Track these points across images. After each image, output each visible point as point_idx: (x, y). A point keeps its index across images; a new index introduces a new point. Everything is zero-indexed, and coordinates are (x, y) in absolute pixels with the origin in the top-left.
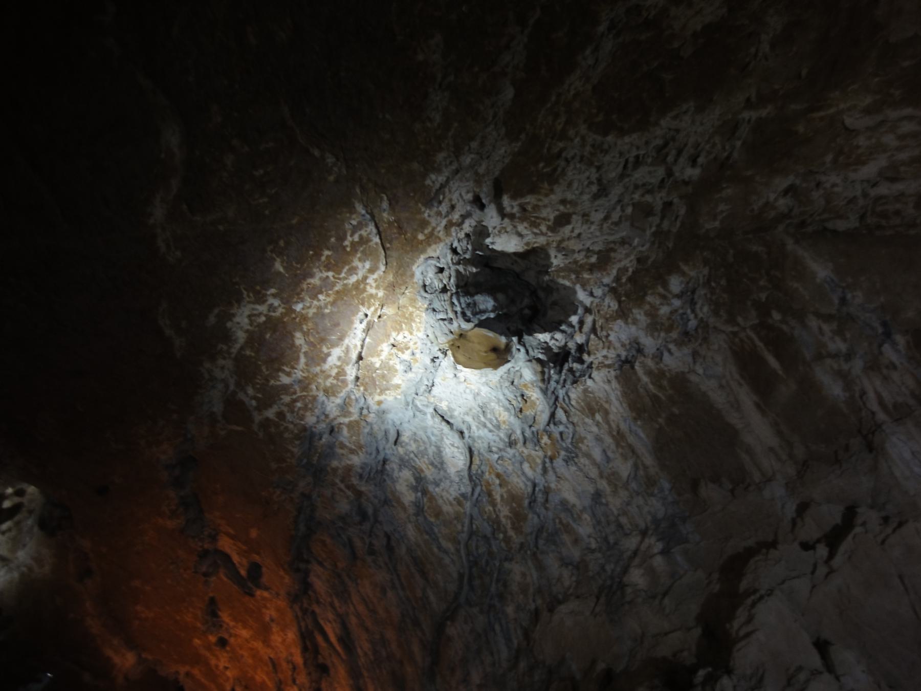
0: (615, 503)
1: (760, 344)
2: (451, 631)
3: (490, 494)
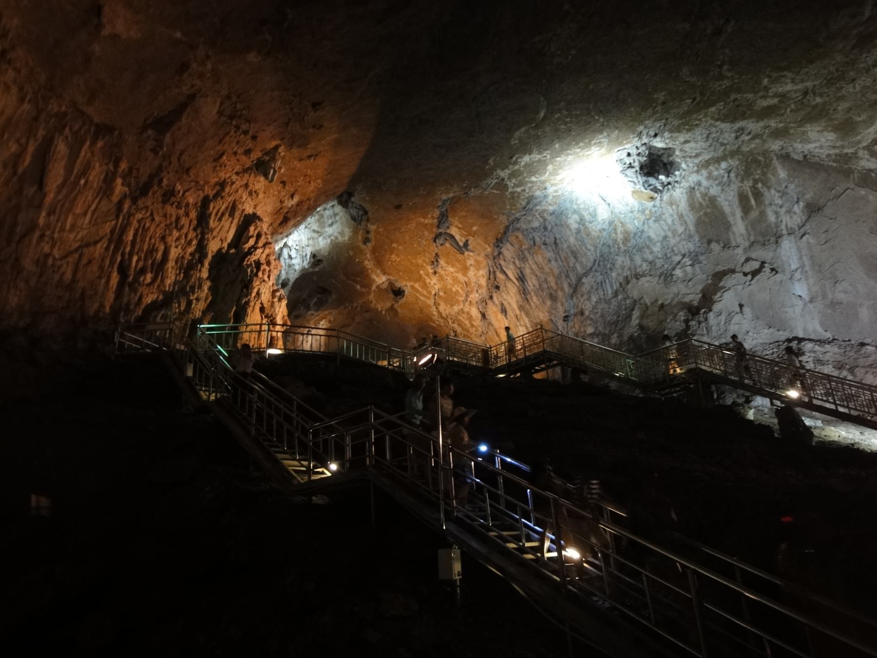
0: (673, 242)
1: (750, 194)
2: (584, 280)
3: (615, 229)
